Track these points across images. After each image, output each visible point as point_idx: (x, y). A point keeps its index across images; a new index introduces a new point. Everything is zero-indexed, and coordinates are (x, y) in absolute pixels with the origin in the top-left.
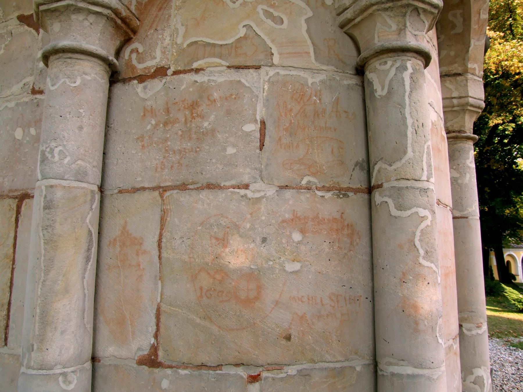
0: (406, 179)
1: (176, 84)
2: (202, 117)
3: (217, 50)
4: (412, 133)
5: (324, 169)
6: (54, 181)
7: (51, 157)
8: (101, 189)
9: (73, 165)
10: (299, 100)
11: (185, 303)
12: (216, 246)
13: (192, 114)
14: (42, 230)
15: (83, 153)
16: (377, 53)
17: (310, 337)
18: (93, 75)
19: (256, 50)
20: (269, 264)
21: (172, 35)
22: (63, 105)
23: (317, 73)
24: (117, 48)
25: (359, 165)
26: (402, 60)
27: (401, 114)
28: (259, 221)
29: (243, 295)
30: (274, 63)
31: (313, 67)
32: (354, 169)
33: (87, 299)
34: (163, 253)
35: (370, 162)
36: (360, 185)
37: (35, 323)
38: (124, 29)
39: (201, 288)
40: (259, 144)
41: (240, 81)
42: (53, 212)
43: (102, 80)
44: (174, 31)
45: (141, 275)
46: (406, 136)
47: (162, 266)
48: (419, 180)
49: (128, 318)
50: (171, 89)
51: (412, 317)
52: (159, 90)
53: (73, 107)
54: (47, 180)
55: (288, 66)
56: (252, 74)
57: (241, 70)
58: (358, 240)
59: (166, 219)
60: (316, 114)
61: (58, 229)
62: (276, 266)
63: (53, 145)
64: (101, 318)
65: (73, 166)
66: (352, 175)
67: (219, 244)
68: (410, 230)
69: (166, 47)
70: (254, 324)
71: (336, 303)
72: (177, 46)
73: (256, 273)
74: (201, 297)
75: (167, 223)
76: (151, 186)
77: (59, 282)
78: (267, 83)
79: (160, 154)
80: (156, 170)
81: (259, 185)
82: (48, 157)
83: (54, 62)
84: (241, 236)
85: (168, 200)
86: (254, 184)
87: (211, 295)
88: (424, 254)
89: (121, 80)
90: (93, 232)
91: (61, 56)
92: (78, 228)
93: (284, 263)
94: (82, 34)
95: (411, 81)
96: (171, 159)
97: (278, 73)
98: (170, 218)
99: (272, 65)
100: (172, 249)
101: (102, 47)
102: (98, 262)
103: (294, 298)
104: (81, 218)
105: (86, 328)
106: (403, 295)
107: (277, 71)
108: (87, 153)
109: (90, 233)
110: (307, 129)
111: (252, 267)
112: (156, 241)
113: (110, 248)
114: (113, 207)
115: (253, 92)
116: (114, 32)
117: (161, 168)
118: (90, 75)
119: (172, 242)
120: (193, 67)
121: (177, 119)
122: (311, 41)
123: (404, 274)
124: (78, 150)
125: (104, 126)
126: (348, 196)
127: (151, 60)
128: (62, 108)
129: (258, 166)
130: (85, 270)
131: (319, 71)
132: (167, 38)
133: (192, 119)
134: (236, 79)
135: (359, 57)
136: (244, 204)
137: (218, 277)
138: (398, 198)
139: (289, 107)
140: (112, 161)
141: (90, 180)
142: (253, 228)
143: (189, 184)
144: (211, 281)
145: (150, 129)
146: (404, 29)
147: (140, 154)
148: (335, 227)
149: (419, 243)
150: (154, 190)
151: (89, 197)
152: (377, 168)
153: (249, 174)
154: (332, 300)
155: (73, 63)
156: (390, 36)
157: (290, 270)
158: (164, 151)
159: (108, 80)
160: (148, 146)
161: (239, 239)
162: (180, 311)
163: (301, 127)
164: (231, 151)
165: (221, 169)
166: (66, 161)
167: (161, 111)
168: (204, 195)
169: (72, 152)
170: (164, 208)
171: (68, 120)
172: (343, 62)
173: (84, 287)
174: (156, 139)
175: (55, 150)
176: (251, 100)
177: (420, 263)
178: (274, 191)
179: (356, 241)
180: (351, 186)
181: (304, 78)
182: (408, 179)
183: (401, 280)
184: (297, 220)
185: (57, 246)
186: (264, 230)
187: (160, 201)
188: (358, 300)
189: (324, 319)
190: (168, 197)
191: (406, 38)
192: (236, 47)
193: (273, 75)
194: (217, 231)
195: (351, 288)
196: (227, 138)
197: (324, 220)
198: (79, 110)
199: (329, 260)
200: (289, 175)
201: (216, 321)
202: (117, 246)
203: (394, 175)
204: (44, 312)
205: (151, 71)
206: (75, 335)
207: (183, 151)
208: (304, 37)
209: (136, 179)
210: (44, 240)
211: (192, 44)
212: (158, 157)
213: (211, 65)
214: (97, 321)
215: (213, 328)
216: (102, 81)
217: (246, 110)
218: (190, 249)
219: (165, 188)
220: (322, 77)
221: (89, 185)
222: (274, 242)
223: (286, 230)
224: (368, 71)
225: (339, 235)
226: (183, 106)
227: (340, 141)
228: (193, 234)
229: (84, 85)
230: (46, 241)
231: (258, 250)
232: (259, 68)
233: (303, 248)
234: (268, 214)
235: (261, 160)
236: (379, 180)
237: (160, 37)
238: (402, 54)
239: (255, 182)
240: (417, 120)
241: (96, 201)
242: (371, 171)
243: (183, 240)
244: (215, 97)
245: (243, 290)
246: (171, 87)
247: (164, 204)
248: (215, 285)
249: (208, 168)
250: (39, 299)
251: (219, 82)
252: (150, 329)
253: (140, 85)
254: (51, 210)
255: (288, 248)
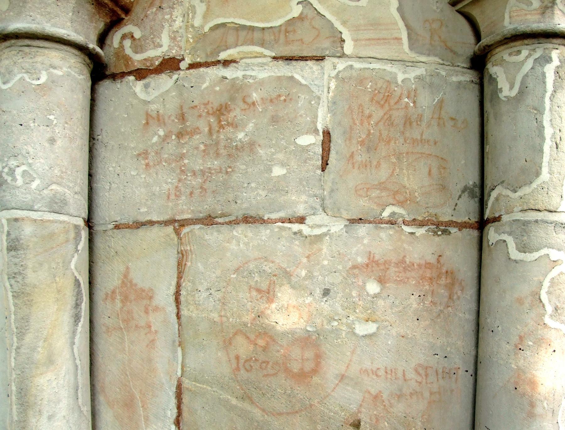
0: (536, 210)
1: (194, 81)
2: (235, 125)
3: (257, 35)
4: (550, 147)
5: (416, 196)
6: (19, 212)
7: (12, 180)
8: (89, 223)
9: (45, 191)
10: (382, 102)
11: (215, 378)
12: (257, 300)
13: (220, 121)
14: (9, 278)
15: (58, 175)
16: (506, 39)
17: (386, 423)
18: (65, 69)
19: (318, 36)
20: (332, 324)
21: (186, 15)
22: (23, 110)
23: (412, 66)
24: (100, 32)
25: (468, 190)
26: (544, 49)
27: (537, 122)
28: (319, 266)
29: (295, 367)
30: (345, 52)
31: (406, 59)
32: (460, 197)
33: (79, 372)
34: (183, 310)
35: (485, 187)
36: (467, 218)
37: (11, 405)
38: (110, 6)
39: (237, 358)
40: (321, 162)
41: (292, 78)
42: (21, 254)
43: (79, 76)
44: (188, 9)
45: (153, 340)
46: (541, 151)
47: (182, 328)
48: (555, 212)
49: (138, 397)
50: (187, 88)
51: (527, 397)
52: (167, 89)
53: (39, 113)
54: (9, 211)
55: (366, 56)
56: (311, 68)
57: (294, 63)
58: (459, 293)
59: (185, 264)
60: (408, 122)
61: (31, 277)
62: (342, 328)
63: (13, 164)
64: (101, 398)
65: (45, 192)
66: (456, 204)
67: (261, 298)
68: (535, 279)
69: (177, 32)
70: (311, 405)
71: (424, 377)
72: (195, 30)
73: (314, 337)
74: (238, 369)
75: (187, 269)
76: (161, 219)
77: (39, 349)
78: (334, 80)
79: (173, 176)
80: (168, 198)
81: (320, 218)
82: (6, 180)
83: (4, 51)
84: (293, 287)
85: (187, 238)
86: (313, 217)
87: (251, 367)
88: (553, 311)
89: (109, 75)
90: (82, 282)
91: (14, 43)
92: (59, 277)
93: (354, 324)
94: (44, 13)
95: (556, 77)
96: (189, 182)
97: (351, 66)
98: (191, 263)
99: (343, 56)
100: (195, 304)
101: (76, 31)
102: (91, 322)
103: (366, 370)
104: (63, 263)
105: (81, 412)
106: (517, 366)
107: (350, 63)
108: (64, 174)
109: (77, 283)
110: (393, 142)
111: (309, 329)
112: (172, 294)
113: (108, 303)
114: (107, 247)
115: (313, 92)
116: (94, 10)
117: (176, 195)
118: (61, 68)
119: (194, 295)
120: (219, 58)
121: (198, 128)
122: (405, 23)
123: (521, 338)
124: (51, 171)
125: (87, 137)
126: (450, 232)
127: (154, 49)
128: (22, 114)
129: (318, 192)
130: (74, 332)
131: (414, 64)
132: (177, 19)
133: (220, 128)
134: (286, 75)
135: (478, 45)
136: (298, 244)
137: (261, 342)
138: (523, 235)
139: (367, 112)
140: (101, 185)
141: (72, 211)
142: (310, 276)
143: (217, 217)
144: (251, 347)
145: (156, 143)
146: (552, 7)
147: (143, 176)
148: (428, 275)
149: (547, 296)
150: (166, 225)
151: (72, 235)
152: (494, 194)
153: (306, 202)
154: (419, 374)
155: (33, 53)
156: (529, 17)
157: (361, 333)
158: (178, 171)
159: (89, 75)
160: (155, 165)
161: (290, 291)
162: (210, 388)
163: (385, 139)
164: (278, 171)
165: (264, 196)
166: (34, 185)
167: (173, 118)
168: (240, 232)
169: (42, 173)
170: (182, 249)
171: (32, 130)
172: (452, 51)
173: (74, 356)
174: (166, 156)
175: (16, 171)
176: (310, 103)
177: (544, 324)
178: (342, 226)
179: (456, 293)
180: (454, 220)
181: (391, 73)
182: (539, 210)
183: (516, 346)
184: (374, 265)
185: (32, 300)
186: (326, 279)
187: (176, 239)
188: (455, 373)
189: (407, 399)
190: (186, 235)
191: (553, 18)
192: (287, 31)
193: (344, 69)
194: (259, 280)
195: (446, 357)
196: (273, 154)
197: (413, 265)
198: (48, 117)
199: (418, 319)
200: (364, 204)
201: (258, 403)
202: (116, 300)
203: (518, 205)
204: (21, 389)
205: (155, 63)
206: (67, 421)
207: (207, 172)
208: (394, 17)
209: (139, 209)
210: (12, 292)
211: (217, 27)
212: (170, 180)
213: (247, 56)
214: (96, 403)
215: (254, 411)
216: (79, 77)
217: (301, 116)
218: (220, 304)
219: (182, 222)
220: (420, 71)
221: (71, 217)
222: (340, 295)
223: (358, 279)
224: (491, 63)
225: (433, 286)
226: (206, 111)
227: (442, 159)
228: (225, 284)
229: (53, 82)
230: (15, 294)
231: (318, 306)
232: (322, 60)
233: (381, 303)
234: (332, 257)
235: (323, 184)
236: (496, 212)
237: (167, 17)
238: (545, 40)
239: (314, 214)
240: (560, 130)
241: (83, 239)
242: (485, 198)
243: (211, 292)
244: (254, 98)
245: (296, 360)
246: (186, 85)
247: (181, 244)
248: (257, 354)
249: (245, 194)
250: (14, 373)
251: (261, 78)
252: (169, 413)
253: (138, 82)
254: (19, 252)
255: (360, 303)
